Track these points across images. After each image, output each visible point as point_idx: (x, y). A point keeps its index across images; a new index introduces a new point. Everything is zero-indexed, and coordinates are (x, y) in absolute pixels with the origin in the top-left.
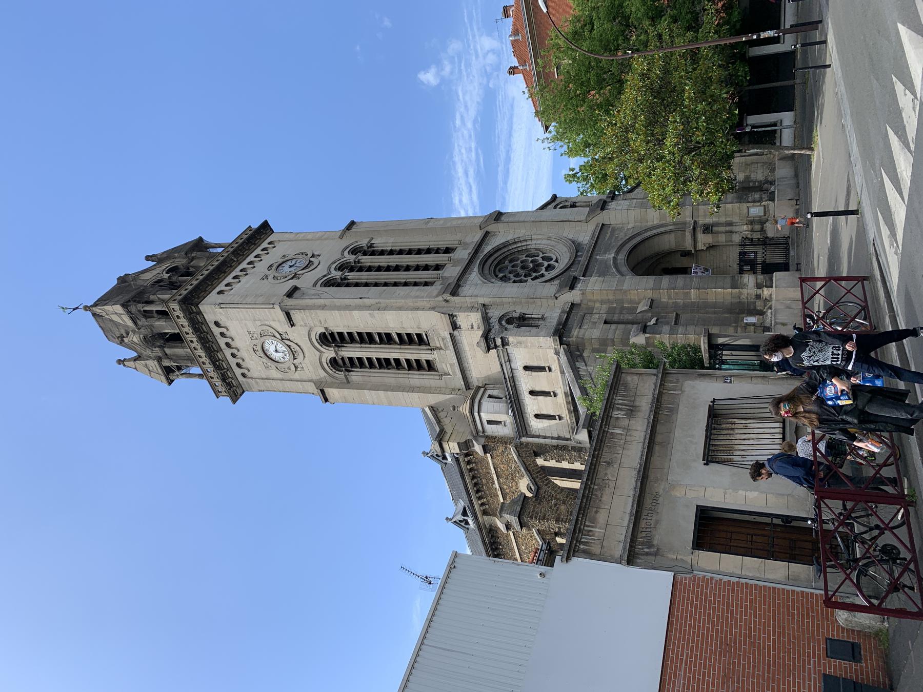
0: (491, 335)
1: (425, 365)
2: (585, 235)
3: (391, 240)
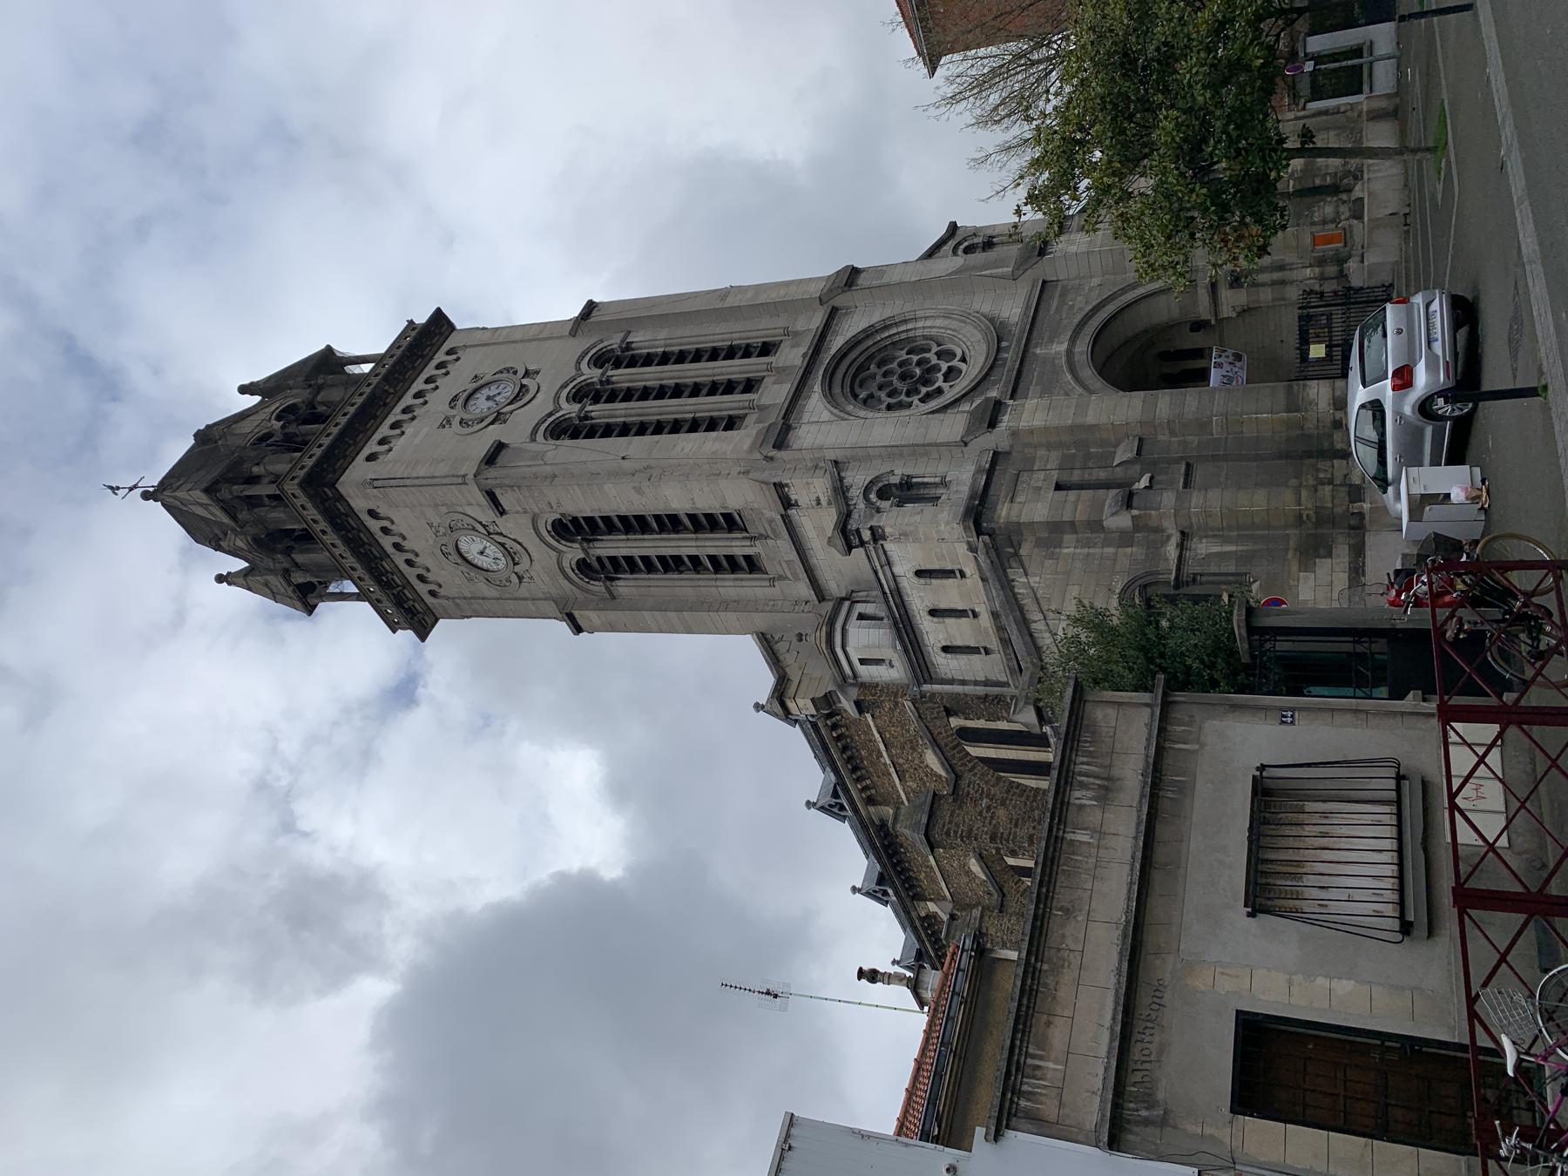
0: (853, 525)
2: (1012, 310)
3: (663, 334)
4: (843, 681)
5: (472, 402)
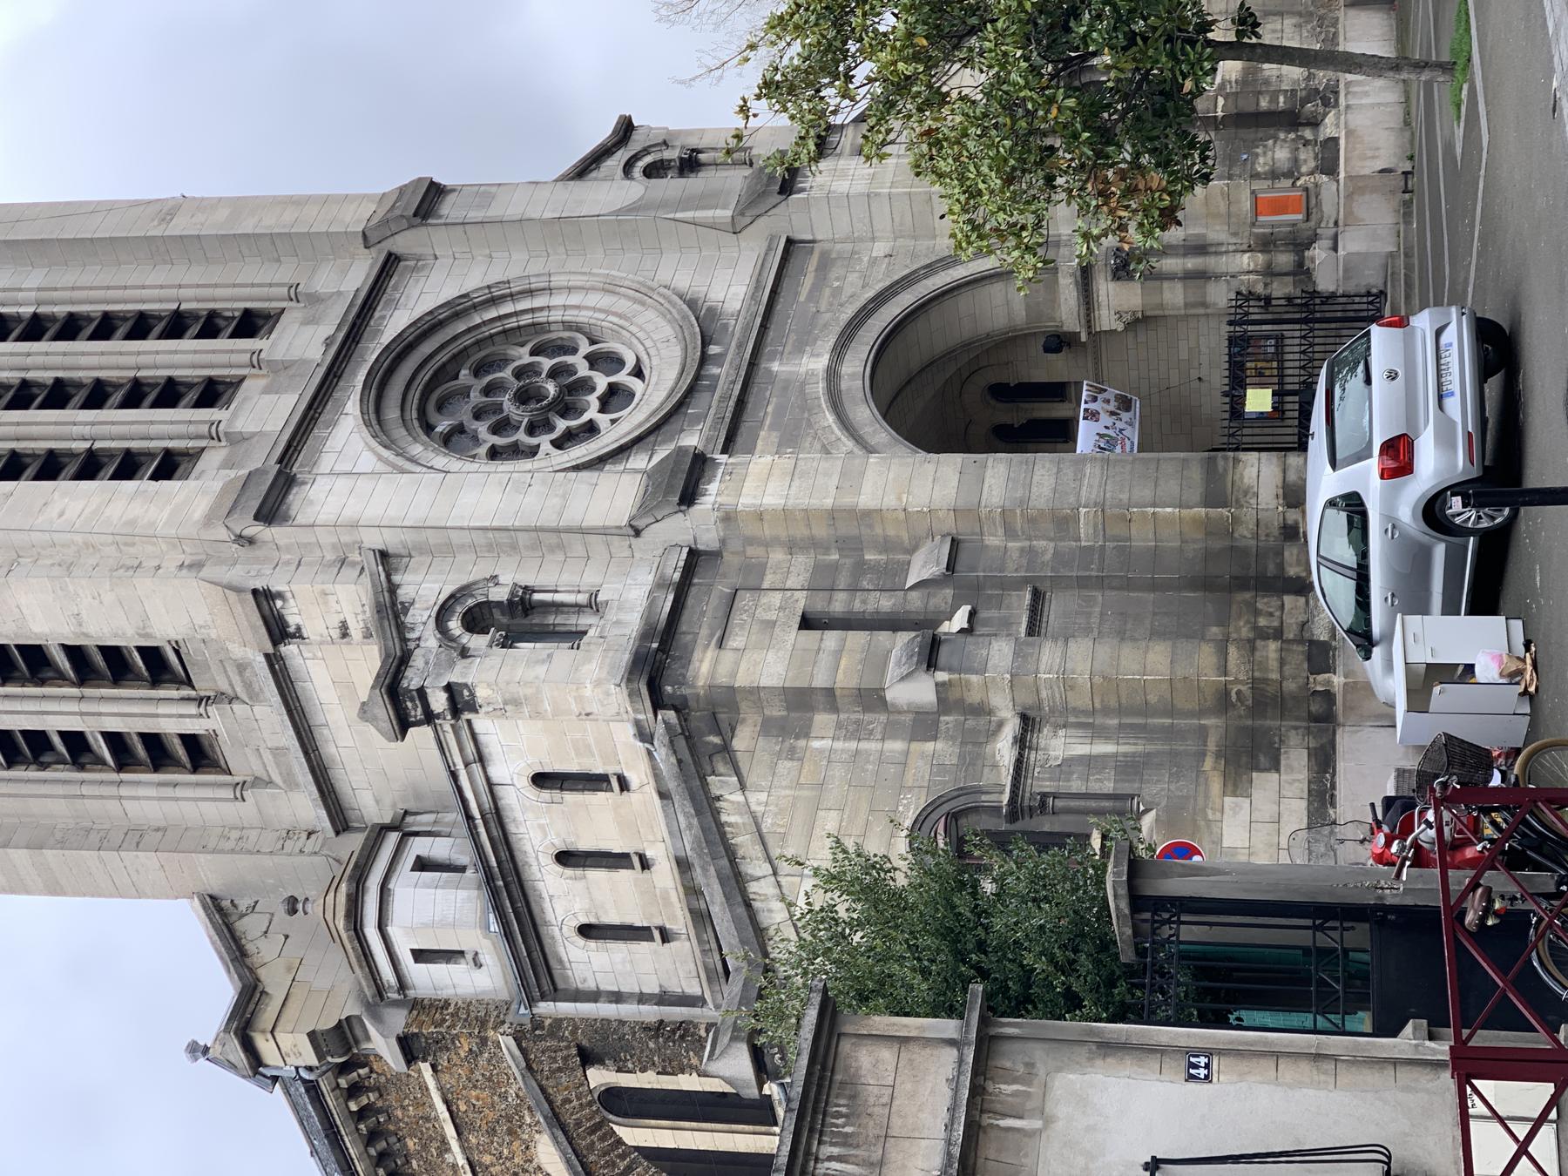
0: (412, 680)
1: (180, 751)
2: (731, 287)
4: (378, 996)
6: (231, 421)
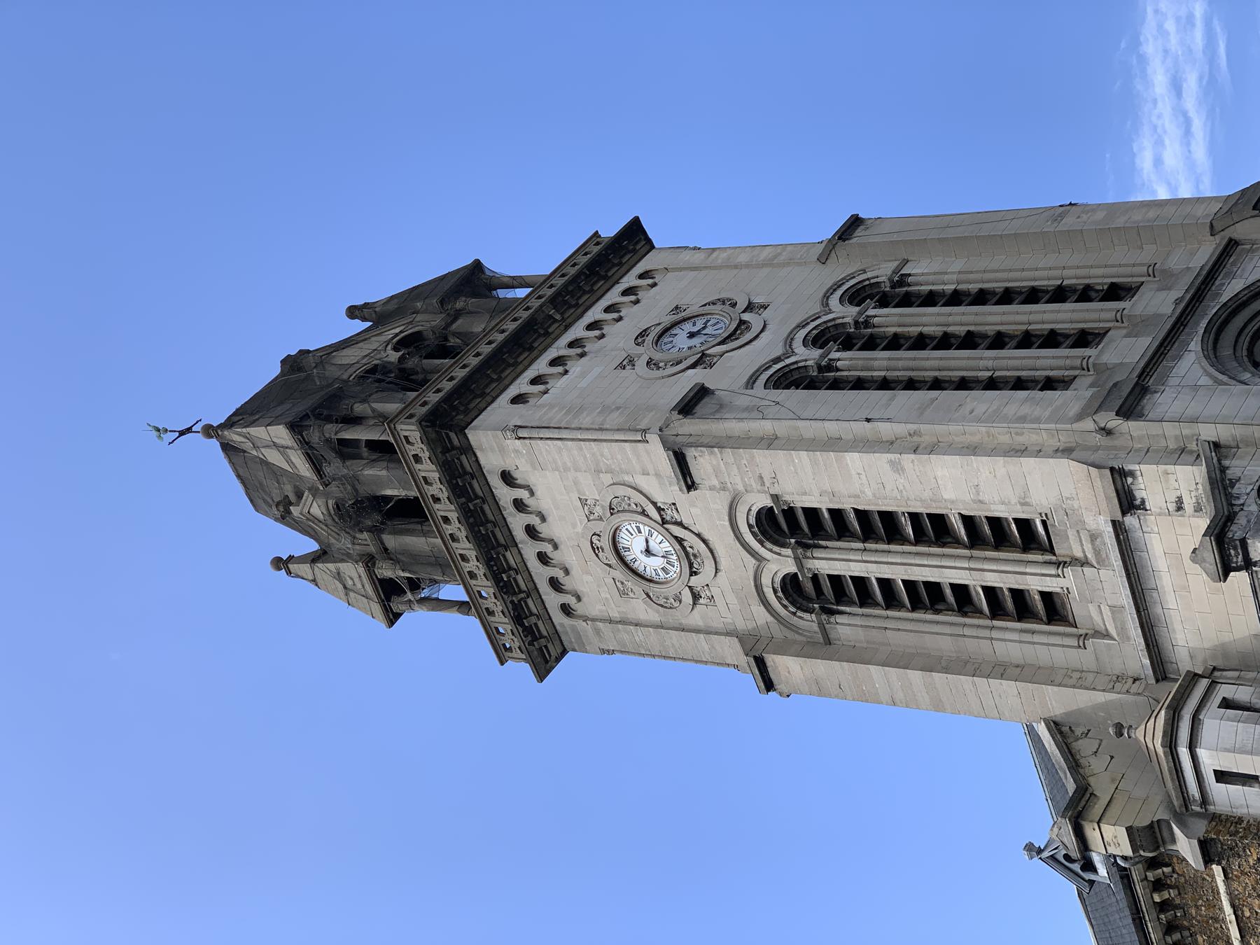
0: (1236, 532)
3: (957, 265)
5: (666, 339)
6: (1098, 356)
